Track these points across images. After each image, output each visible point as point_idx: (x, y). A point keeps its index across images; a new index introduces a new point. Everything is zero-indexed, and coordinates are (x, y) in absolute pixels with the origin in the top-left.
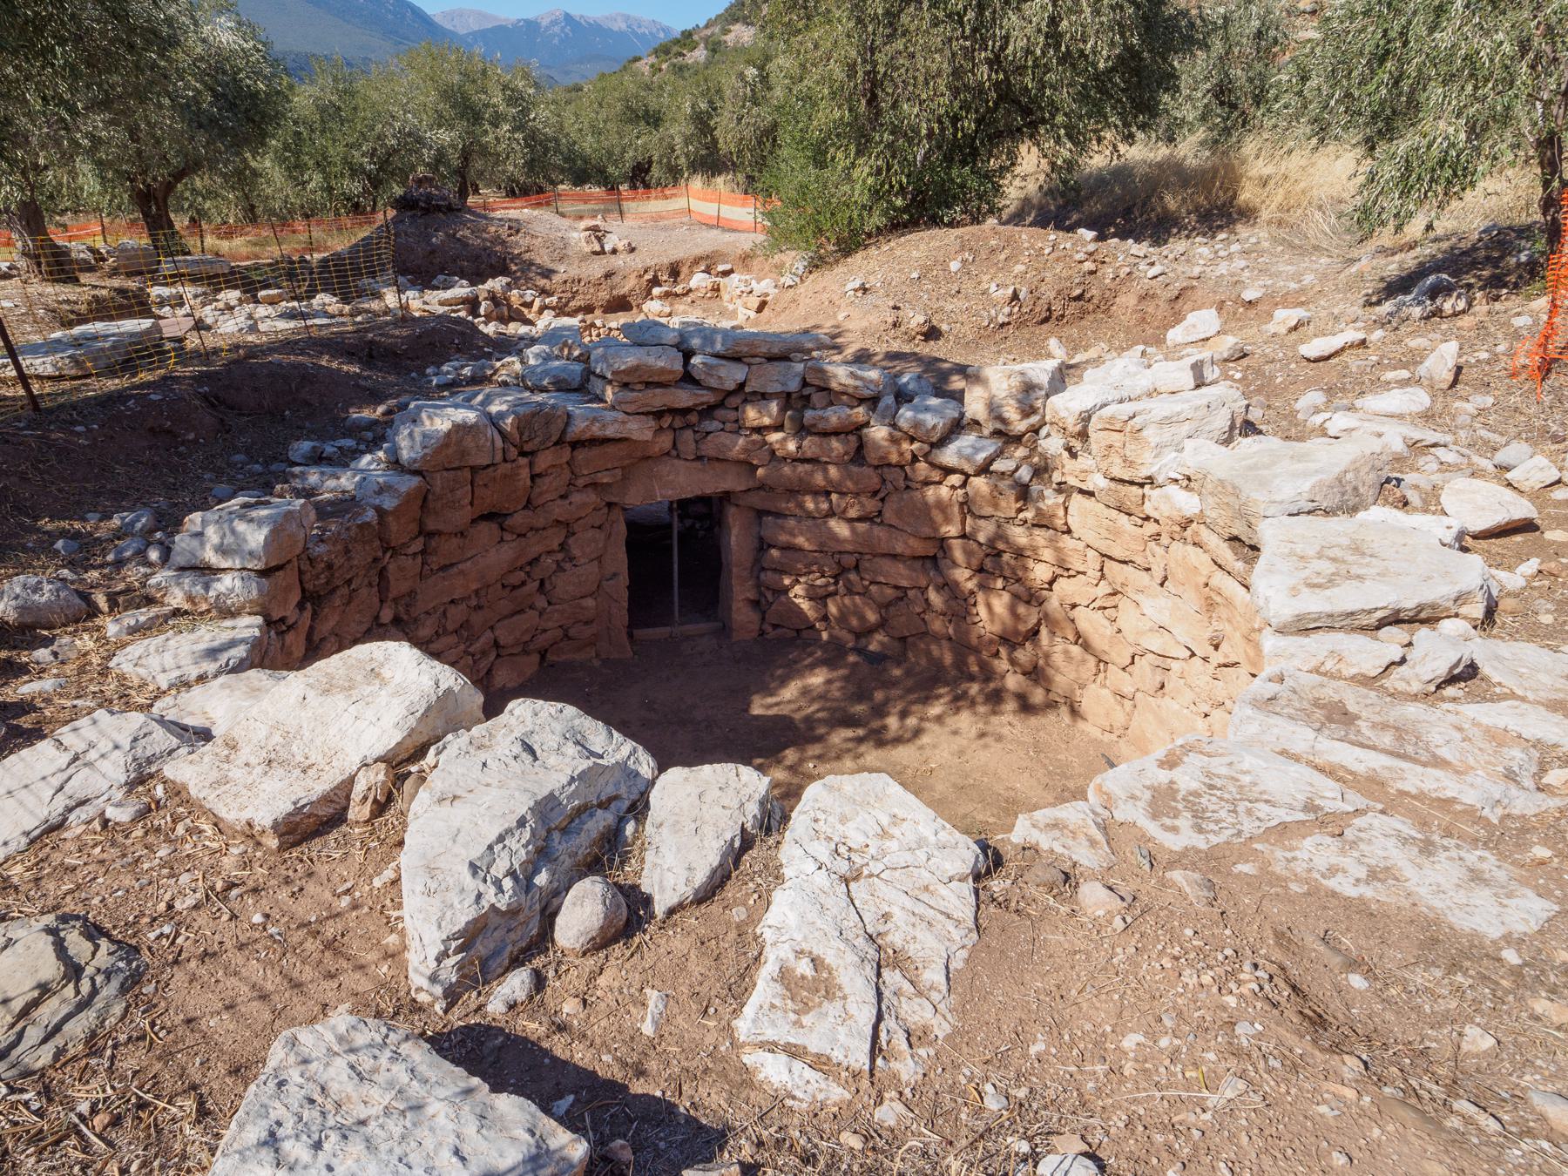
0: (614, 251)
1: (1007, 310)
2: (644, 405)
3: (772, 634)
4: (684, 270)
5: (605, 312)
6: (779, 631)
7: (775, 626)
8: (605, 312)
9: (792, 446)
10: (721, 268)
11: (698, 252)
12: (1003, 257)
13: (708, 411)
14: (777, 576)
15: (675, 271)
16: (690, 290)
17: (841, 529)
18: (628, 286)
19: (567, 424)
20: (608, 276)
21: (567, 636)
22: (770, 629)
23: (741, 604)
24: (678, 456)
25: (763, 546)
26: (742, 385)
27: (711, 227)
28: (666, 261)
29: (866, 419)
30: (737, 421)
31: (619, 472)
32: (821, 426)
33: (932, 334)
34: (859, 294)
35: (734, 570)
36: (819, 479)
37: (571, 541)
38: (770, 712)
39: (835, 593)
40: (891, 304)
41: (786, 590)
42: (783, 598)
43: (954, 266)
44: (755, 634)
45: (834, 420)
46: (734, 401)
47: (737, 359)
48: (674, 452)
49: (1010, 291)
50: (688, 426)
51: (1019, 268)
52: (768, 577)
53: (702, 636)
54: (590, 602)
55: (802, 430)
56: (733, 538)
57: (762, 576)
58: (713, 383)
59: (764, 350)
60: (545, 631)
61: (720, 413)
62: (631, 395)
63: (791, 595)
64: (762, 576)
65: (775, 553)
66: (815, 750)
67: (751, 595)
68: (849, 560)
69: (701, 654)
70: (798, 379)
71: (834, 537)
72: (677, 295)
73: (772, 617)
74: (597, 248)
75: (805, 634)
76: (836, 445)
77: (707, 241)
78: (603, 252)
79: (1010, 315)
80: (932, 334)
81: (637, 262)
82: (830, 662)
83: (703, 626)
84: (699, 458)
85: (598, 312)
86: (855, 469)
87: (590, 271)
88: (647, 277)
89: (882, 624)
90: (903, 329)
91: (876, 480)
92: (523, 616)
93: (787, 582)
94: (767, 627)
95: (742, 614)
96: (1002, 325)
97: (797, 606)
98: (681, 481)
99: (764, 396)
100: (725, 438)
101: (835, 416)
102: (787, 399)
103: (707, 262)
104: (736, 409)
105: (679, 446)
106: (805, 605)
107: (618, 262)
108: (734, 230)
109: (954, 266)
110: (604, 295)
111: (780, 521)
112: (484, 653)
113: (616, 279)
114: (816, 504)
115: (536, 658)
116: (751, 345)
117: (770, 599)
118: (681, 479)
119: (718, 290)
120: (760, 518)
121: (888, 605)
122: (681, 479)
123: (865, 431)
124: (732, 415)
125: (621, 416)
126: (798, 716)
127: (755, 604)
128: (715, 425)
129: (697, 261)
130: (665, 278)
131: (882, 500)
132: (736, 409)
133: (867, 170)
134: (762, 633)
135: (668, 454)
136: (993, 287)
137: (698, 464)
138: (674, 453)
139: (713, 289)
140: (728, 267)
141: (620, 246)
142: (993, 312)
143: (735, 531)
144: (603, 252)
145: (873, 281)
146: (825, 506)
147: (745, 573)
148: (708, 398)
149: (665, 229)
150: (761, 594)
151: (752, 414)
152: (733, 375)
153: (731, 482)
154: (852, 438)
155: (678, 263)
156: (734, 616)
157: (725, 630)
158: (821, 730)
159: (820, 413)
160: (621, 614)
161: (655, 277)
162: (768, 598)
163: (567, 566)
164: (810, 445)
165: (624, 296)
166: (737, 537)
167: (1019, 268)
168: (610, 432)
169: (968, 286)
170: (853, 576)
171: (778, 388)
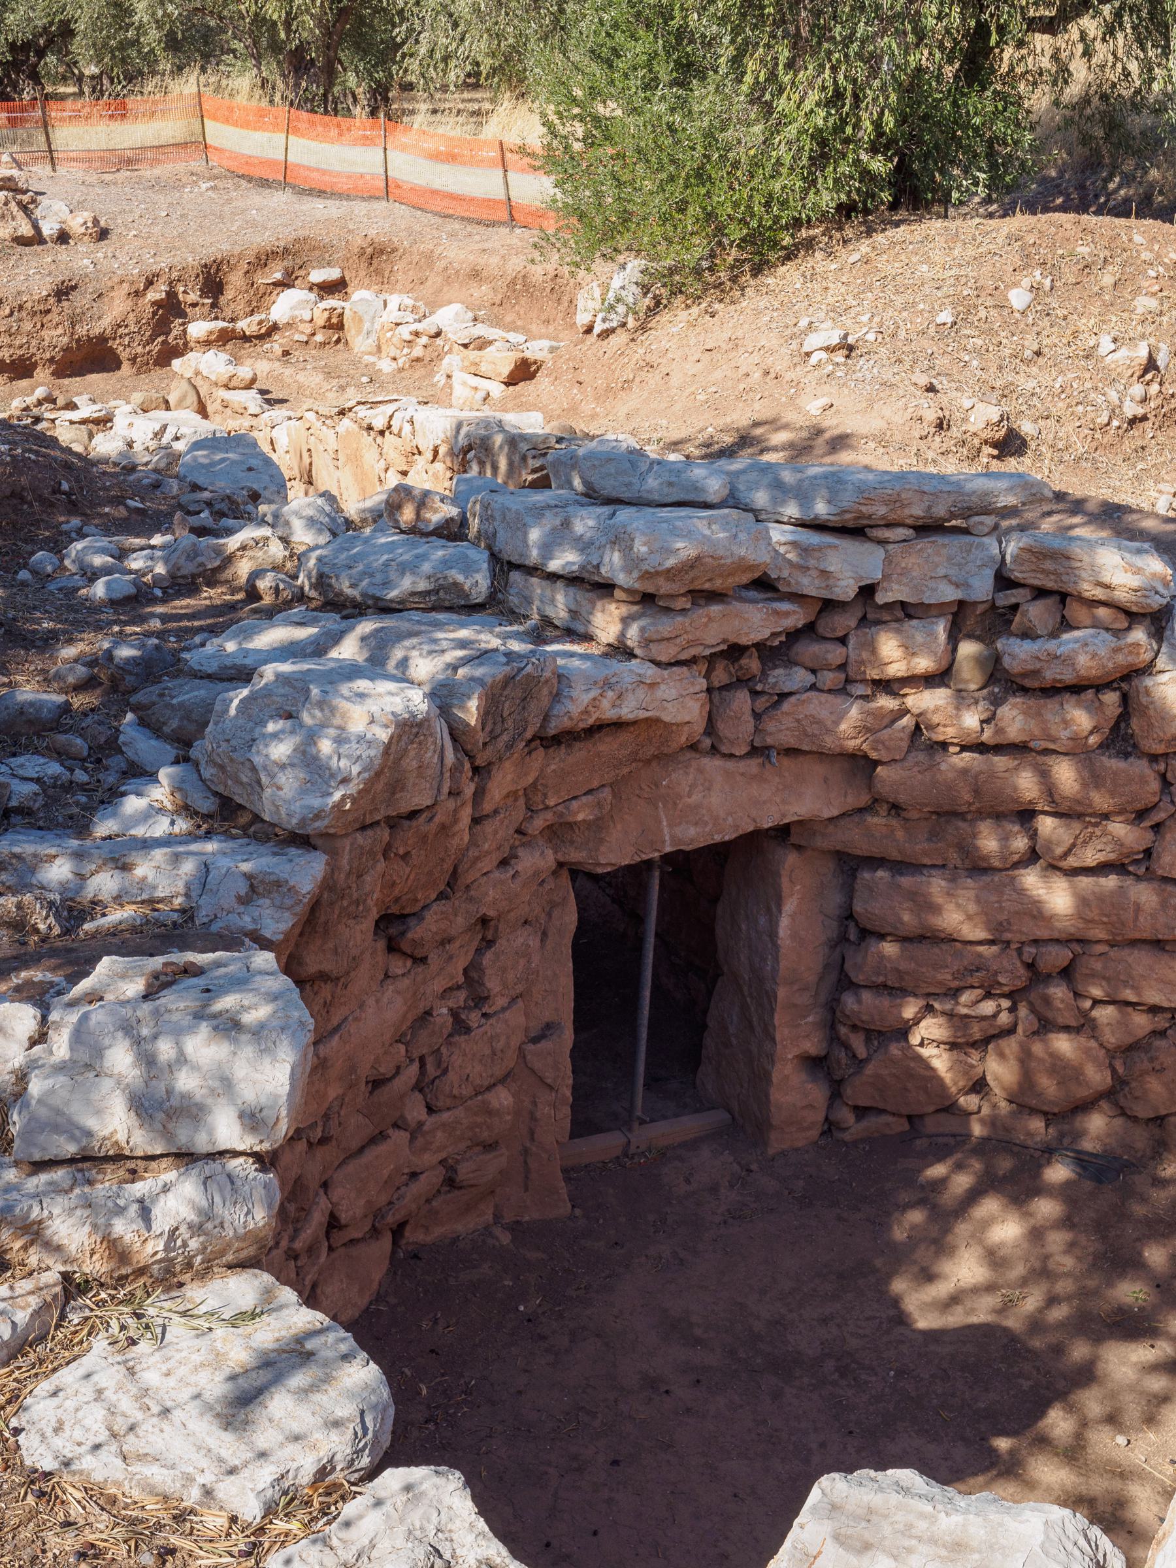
0: (63, 237)
1: (1137, 390)
2: (691, 644)
3: (854, 1128)
4: (235, 281)
5: (59, 374)
6: (873, 1122)
7: (861, 1112)
8: (59, 374)
9: (971, 720)
10: (317, 276)
11: (264, 240)
12: (1107, 280)
13: (775, 652)
14: (885, 1002)
15: (212, 283)
16: (275, 328)
17: (1058, 898)
18: (112, 313)
19: (557, 697)
20: (63, 292)
21: (451, 1182)
22: (846, 1116)
23: (788, 1069)
24: (714, 750)
25: (853, 931)
26: (867, 591)
27: (264, 183)
28: (192, 260)
29: (1147, 656)
30: (843, 667)
31: (606, 794)
32: (1051, 674)
33: (1010, 444)
34: (839, 357)
35: (782, 993)
36: (1026, 784)
37: (487, 959)
38: (955, 1319)
39: (1011, 1031)
40: (923, 380)
41: (903, 1031)
42: (895, 1050)
43: (1018, 298)
44: (814, 1133)
45: (1083, 660)
46: (845, 622)
47: (855, 530)
48: (710, 740)
49: (1143, 352)
50: (742, 682)
51: (1145, 304)
52: (862, 1005)
53: (693, 1145)
54: (502, 1098)
55: (1001, 681)
56: (784, 922)
57: (849, 1002)
58: (809, 585)
59: (917, 511)
60: (414, 1175)
61: (809, 650)
62: (666, 626)
63: (915, 1040)
64: (849, 1002)
65: (889, 948)
66: (1092, 1402)
67: (812, 1045)
68: (1058, 956)
69: (714, 1189)
70: (989, 573)
71: (1036, 911)
72: (245, 338)
73: (858, 1091)
74: (26, 230)
75: (931, 1125)
76: (1080, 718)
77: (274, 217)
78: (37, 239)
79: (1144, 400)
80: (1010, 444)
81: (123, 261)
82: (1019, 1187)
83: (689, 1125)
84: (756, 751)
85: (42, 374)
86: (1113, 764)
87: (18, 283)
88: (153, 295)
89: (1113, 1095)
90: (955, 432)
91: (1155, 785)
92: (382, 1148)
93: (909, 1012)
94: (846, 1116)
95: (794, 1094)
96: (1134, 421)
97: (924, 1063)
98: (713, 804)
99: (907, 611)
100: (817, 706)
101: (1085, 649)
102: (960, 618)
103: (287, 262)
104: (843, 640)
105: (720, 726)
106: (940, 1061)
107: (81, 259)
108: (321, 193)
109: (1018, 298)
110: (56, 336)
111: (906, 881)
112: (311, 1250)
113: (80, 300)
114: (1005, 839)
115: (386, 1242)
116: (895, 501)
117: (861, 1051)
118: (715, 799)
119: (340, 326)
120: (852, 874)
121: (1131, 1049)
122: (715, 799)
123: (1148, 682)
124: (835, 654)
125: (650, 671)
126: (1012, 1322)
127: (815, 1064)
128: (800, 677)
129: (263, 260)
130: (193, 297)
131: (1157, 828)
132: (843, 640)
133: (814, 96)
134: (830, 1127)
135: (693, 747)
136: (1106, 345)
137: (753, 765)
138: (707, 742)
139: (328, 326)
140: (333, 274)
141: (77, 223)
142: (1113, 396)
143: (790, 906)
144: (37, 239)
145: (862, 331)
146: (1020, 843)
147: (804, 999)
148: (796, 617)
149: (157, 185)
150: (834, 1038)
151: (892, 653)
152: (848, 567)
153: (809, 799)
154: (1111, 698)
155: (218, 264)
156: (776, 1095)
157: (747, 1125)
158: (1079, 1351)
159: (1052, 645)
160: (555, 1114)
161: (171, 295)
162: (852, 1047)
163: (474, 1018)
164: (1014, 719)
165: (102, 339)
166: (795, 918)
167: (1145, 304)
168: (628, 711)
169: (1052, 339)
170: (1058, 992)
171: (950, 594)
